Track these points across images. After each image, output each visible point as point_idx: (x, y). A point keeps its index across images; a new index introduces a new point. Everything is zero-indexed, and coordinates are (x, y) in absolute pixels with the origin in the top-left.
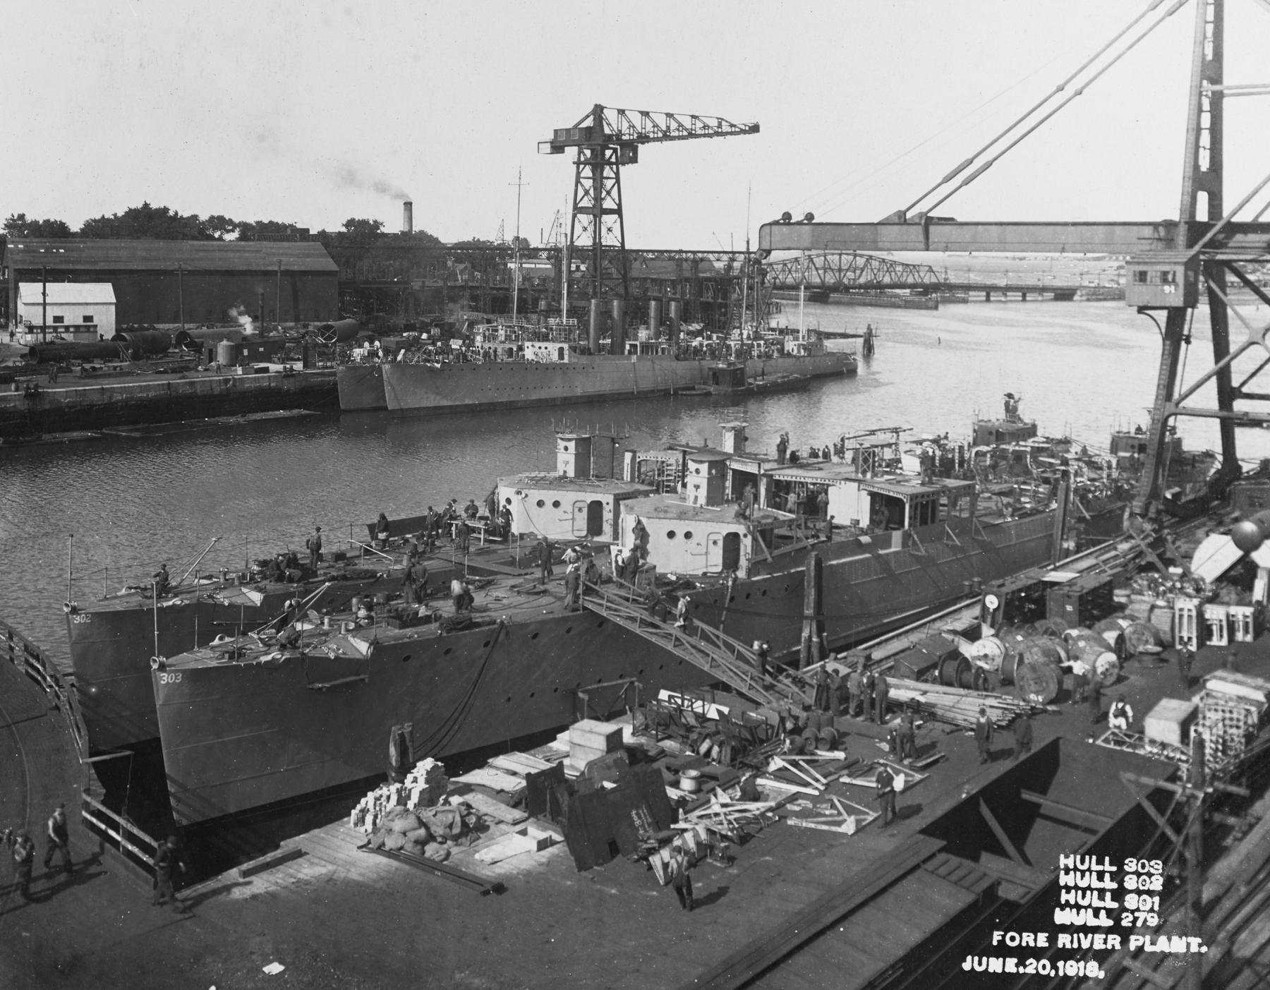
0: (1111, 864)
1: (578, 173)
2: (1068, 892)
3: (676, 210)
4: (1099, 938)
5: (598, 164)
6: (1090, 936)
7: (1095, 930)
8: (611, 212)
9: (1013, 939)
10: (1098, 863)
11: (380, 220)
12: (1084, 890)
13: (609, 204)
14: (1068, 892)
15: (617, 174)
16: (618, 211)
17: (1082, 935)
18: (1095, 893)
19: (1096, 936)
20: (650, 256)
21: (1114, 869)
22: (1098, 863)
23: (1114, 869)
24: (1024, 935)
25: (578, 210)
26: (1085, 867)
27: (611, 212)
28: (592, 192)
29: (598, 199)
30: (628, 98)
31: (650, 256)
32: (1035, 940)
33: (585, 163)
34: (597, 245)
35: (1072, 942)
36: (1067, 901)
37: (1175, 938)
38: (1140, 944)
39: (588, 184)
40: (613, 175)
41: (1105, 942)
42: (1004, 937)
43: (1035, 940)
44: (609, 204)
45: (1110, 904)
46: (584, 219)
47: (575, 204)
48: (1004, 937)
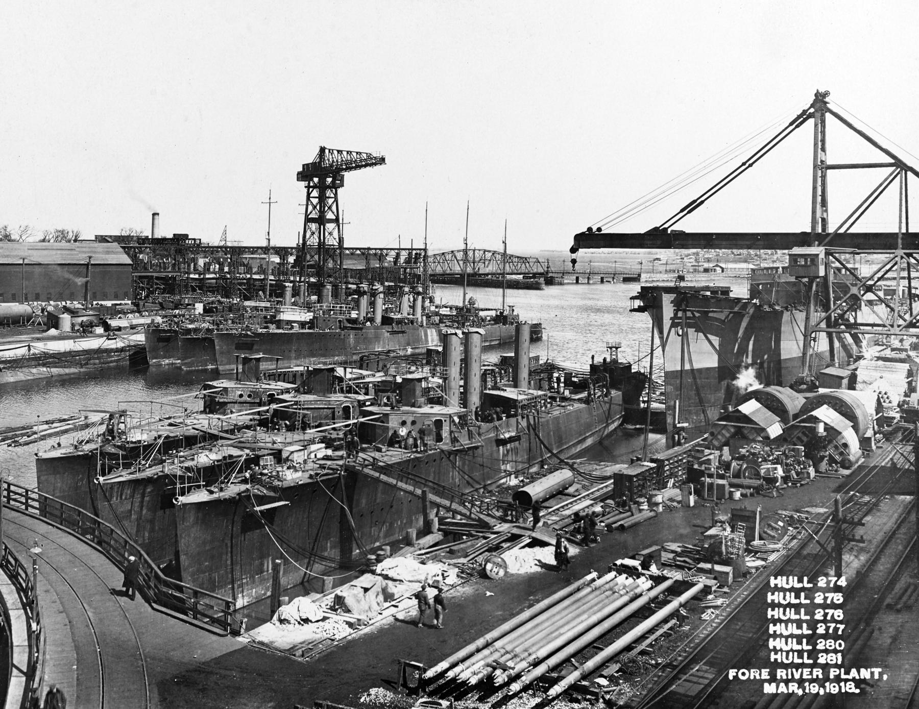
0: (807, 644)
1: (309, 194)
2: (776, 654)
3: (369, 219)
4: (806, 671)
5: (322, 188)
6: (800, 670)
7: (803, 665)
8: (330, 221)
9: (743, 674)
10: (796, 598)
11: (822, 90)
12: (787, 638)
13: (330, 216)
14: (776, 654)
15: (336, 194)
16: (336, 220)
17: (794, 670)
18: (796, 654)
19: (805, 670)
20: (358, 252)
21: (810, 648)
22: (796, 598)
23: (810, 648)
24: (752, 671)
25: (308, 220)
26: (788, 648)
27: (330, 221)
28: (318, 207)
29: (322, 212)
30: (344, 141)
31: (358, 252)
32: (760, 675)
33: (314, 187)
34: (322, 244)
35: (787, 675)
36: (776, 585)
37: (863, 670)
38: (837, 673)
39: (315, 201)
40: (332, 195)
41: (811, 673)
42: (737, 673)
43: (760, 675)
44: (330, 216)
45: (806, 631)
46: (314, 226)
47: (307, 215)
48: (737, 673)
